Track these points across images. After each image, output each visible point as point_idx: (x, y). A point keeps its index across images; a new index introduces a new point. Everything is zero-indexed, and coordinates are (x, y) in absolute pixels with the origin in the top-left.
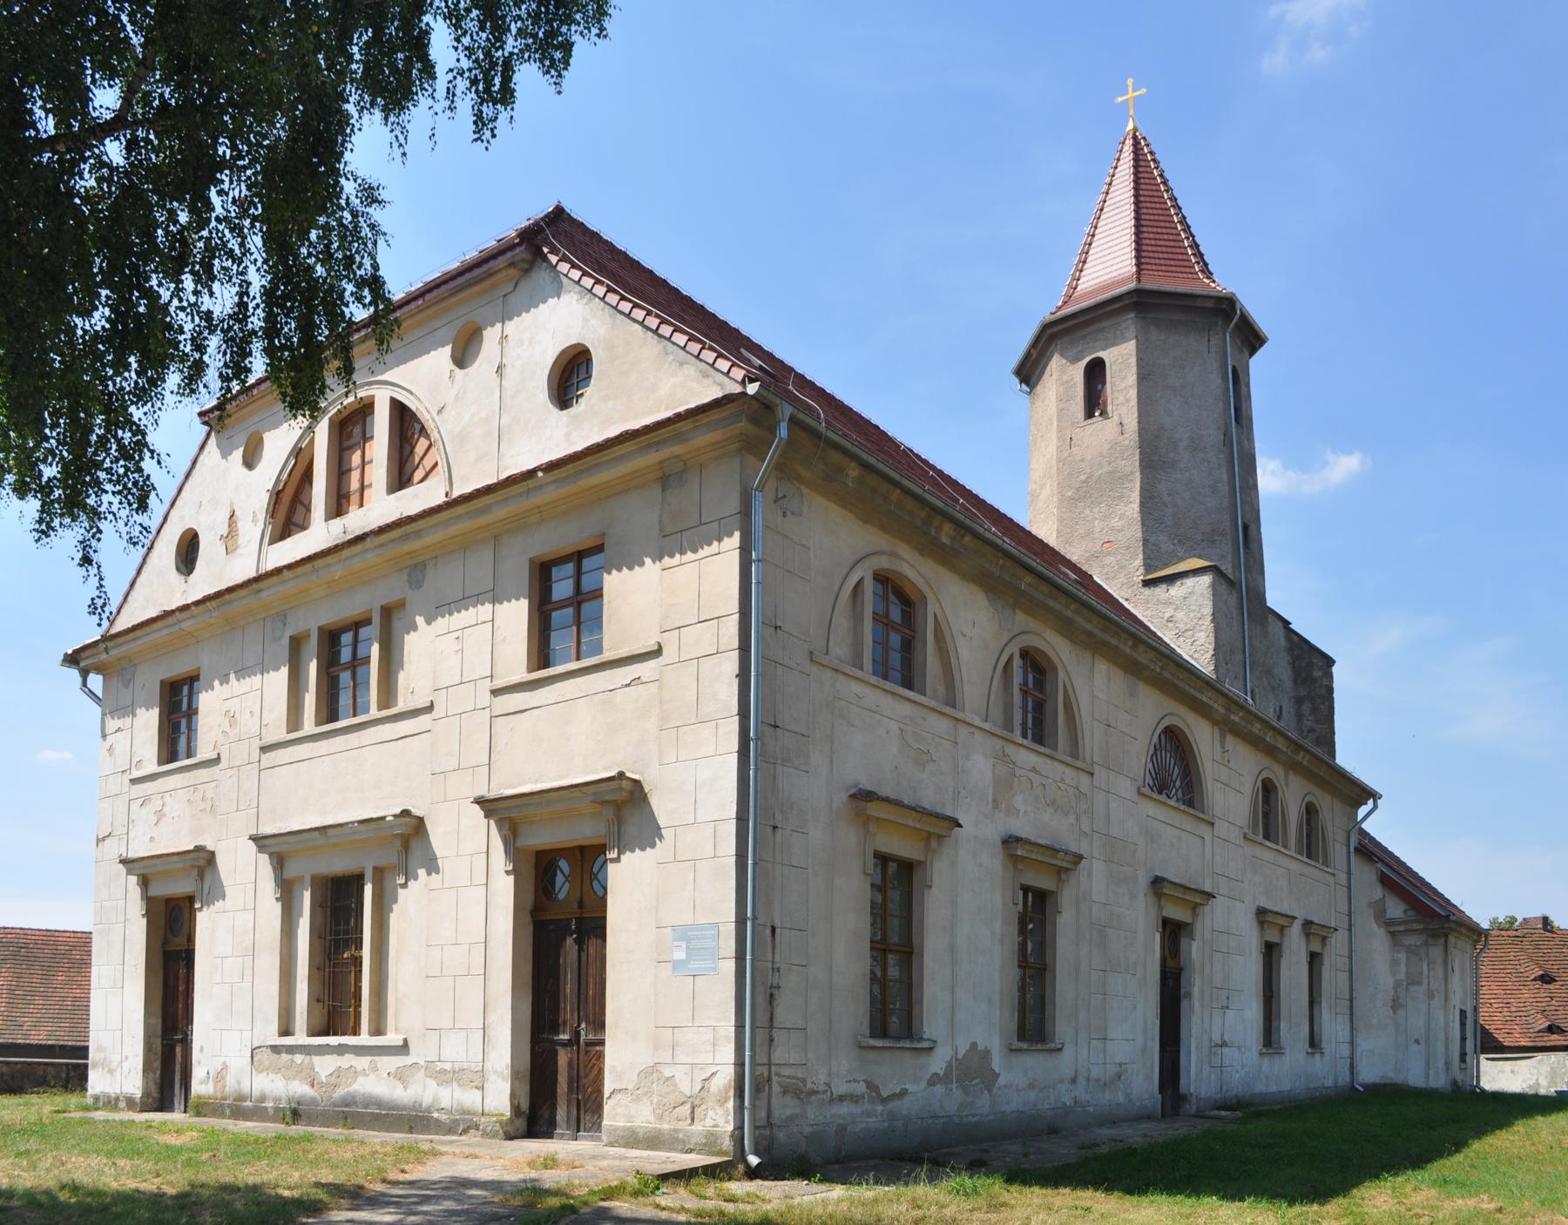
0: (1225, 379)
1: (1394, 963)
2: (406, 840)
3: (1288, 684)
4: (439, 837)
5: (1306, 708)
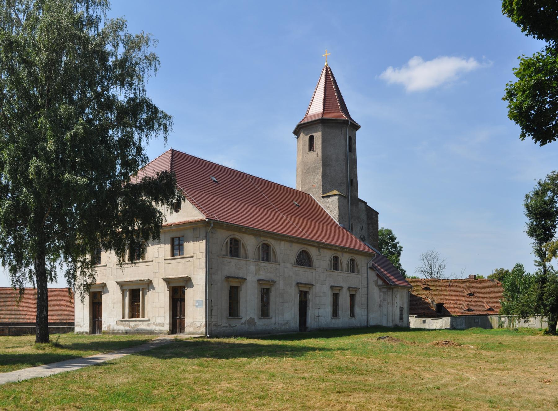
0: (346, 141)
1: (380, 296)
2: (149, 284)
3: (365, 220)
4: (155, 283)
5: (370, 226)
